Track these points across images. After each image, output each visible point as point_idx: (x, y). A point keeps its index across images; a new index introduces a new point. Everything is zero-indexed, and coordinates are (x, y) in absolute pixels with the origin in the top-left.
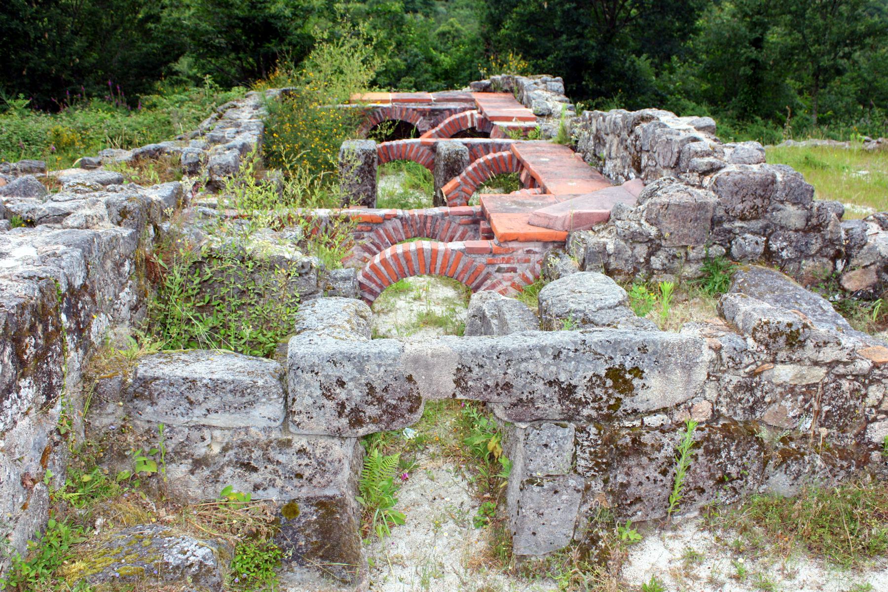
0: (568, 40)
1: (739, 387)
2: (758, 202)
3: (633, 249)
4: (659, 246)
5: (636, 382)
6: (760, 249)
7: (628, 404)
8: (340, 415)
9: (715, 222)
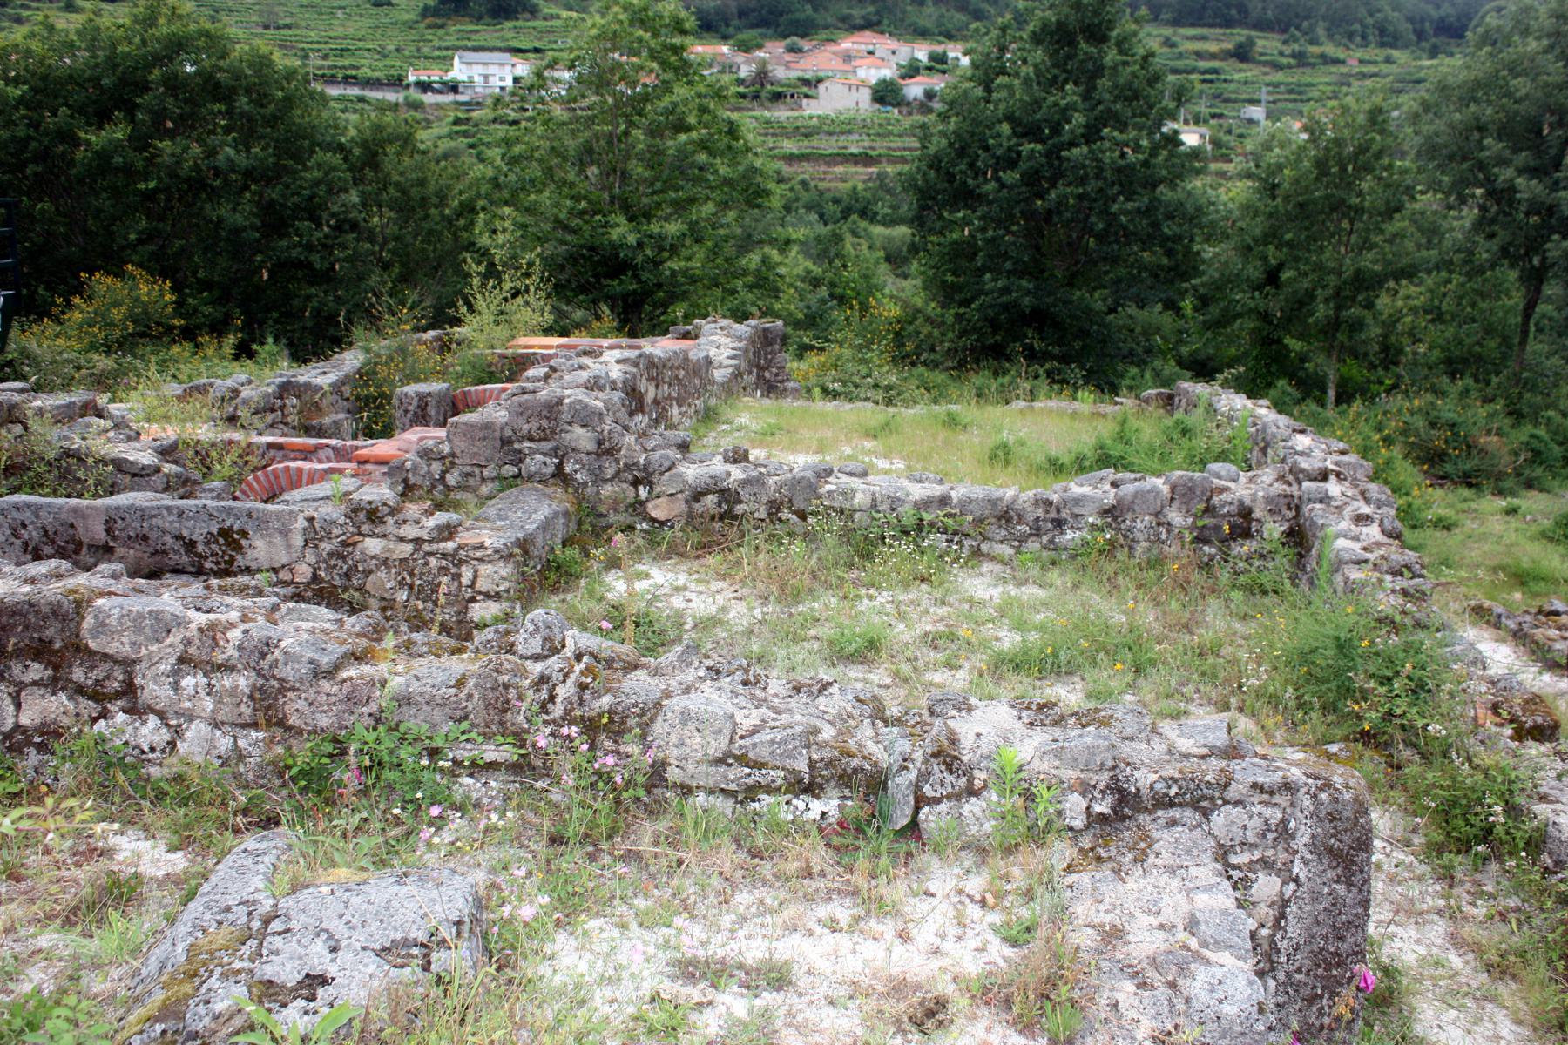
0: (995, 280)
1: (331, 554)
2: (544, 423)
3: (429, 466)
4: (452, 463)
5: (244, 542)
6: (550, 470)
7: (240, 561)
8: (25, 551)
9: (506, 442)
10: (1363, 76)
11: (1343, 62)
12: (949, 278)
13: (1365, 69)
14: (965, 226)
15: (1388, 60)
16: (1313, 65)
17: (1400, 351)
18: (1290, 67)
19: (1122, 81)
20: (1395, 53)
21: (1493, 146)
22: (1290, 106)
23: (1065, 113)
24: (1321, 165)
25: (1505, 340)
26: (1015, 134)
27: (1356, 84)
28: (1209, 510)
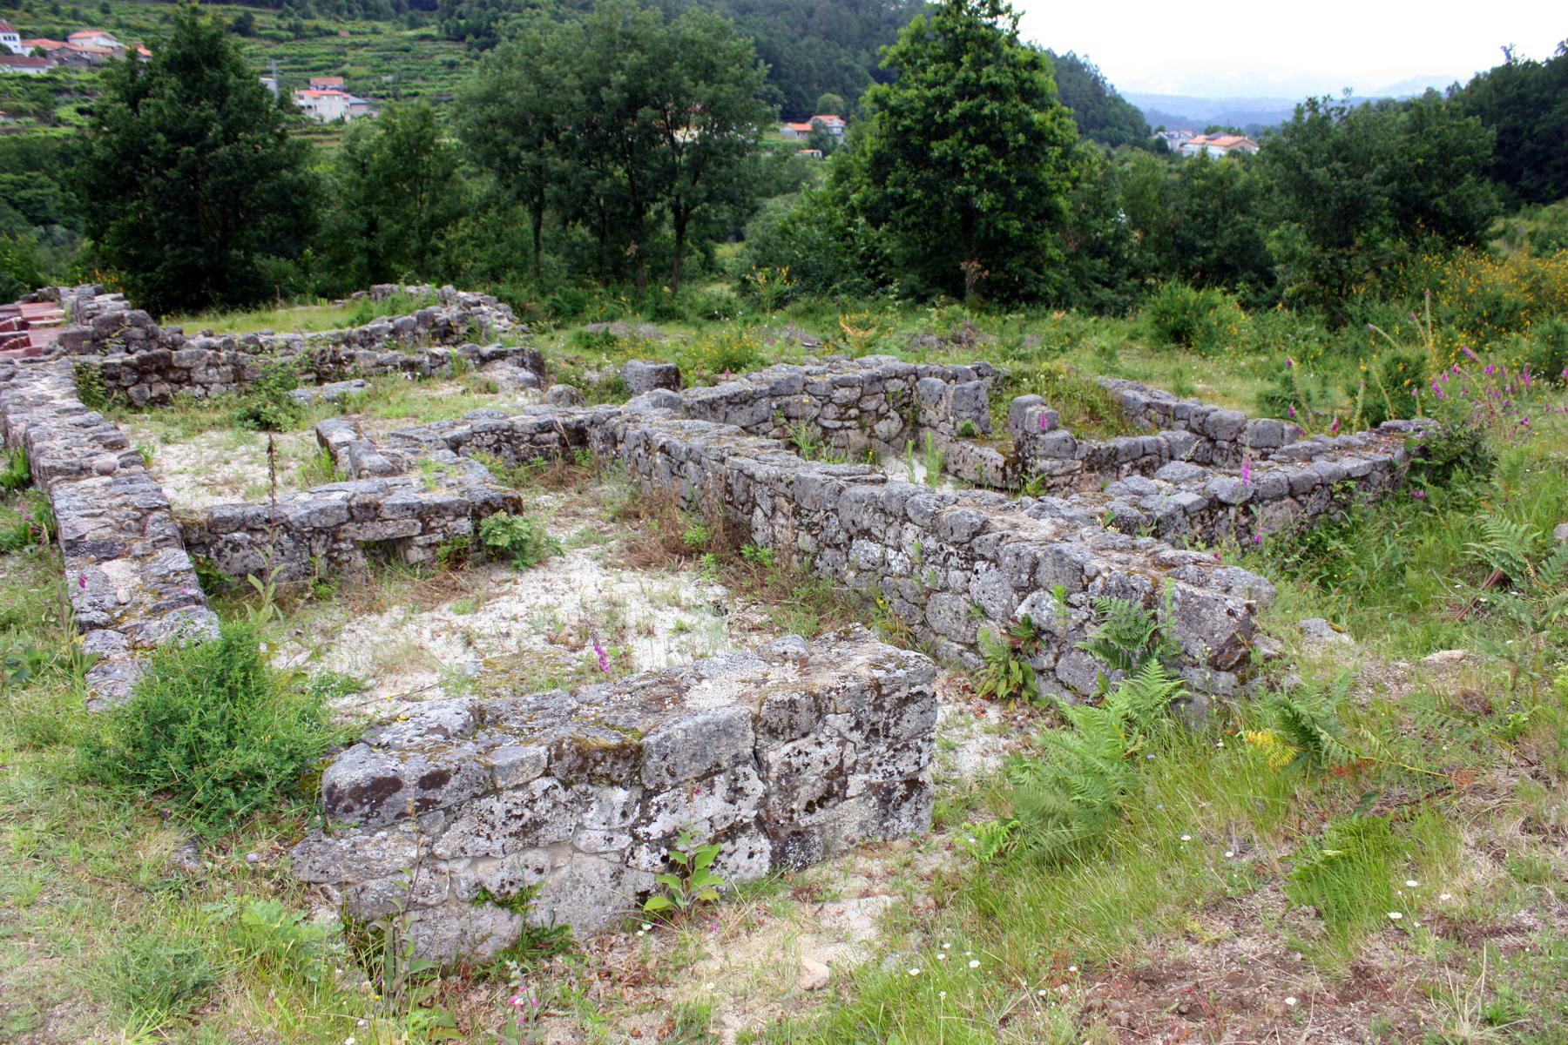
0: (173, 249)
10: (356, 46)
11: (336, 34)
12: (132, 252)
13: (357, 39)
14: (134, 211)
15: (375, 31)
16: (310, 38)
17: (459, 267)
18: (289, 39)
19: (245, 97)
20: (380, 25)
21: (503, 133)
22: (296, 75)
23: (206, 123)
24: (397, 151)
25: (524, 252)
26: (169, 141)
27: (351, 53)
28: (435, 325)
